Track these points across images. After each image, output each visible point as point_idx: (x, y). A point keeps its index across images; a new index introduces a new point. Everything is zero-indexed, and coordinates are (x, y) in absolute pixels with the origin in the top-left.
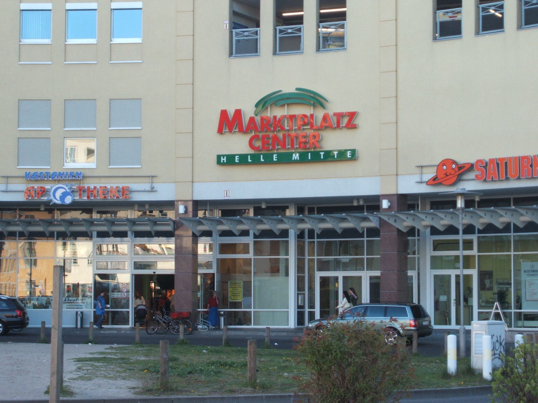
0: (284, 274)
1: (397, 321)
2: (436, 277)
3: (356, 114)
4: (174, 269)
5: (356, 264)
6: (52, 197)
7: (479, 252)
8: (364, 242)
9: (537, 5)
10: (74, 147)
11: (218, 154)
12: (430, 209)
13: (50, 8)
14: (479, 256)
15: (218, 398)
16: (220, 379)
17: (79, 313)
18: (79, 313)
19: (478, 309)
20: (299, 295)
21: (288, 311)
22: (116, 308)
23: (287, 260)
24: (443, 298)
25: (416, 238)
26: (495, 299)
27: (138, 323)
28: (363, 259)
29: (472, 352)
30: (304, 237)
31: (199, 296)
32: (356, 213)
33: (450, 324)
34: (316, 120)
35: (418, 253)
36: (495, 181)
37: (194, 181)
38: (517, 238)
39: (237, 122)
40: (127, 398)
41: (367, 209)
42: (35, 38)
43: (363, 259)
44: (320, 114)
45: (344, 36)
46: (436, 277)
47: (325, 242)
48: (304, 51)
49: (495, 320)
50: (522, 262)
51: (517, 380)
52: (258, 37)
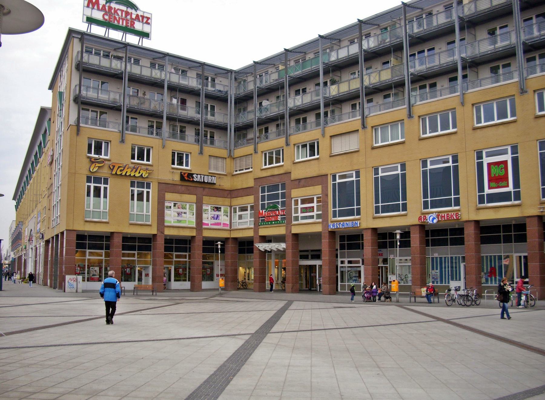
0: (531, 21)
1: (119, 293)
2: (104, 187)
3: (37, 276)
4: (138, 38)
5: (292, 352)
6: (428, 221)
7: (105, 257)
8: (454, 194)
9: (544, 204)
10: (363, 52)
11: (42, 106)
12: (106, 300)
13: (354, 148)
14: (137, 260)
15: (153, 269)
16: (37, 170)
17: (489, 283)
18: (489, 283)
19: (511, 155)
20: (131, 98)
21: (138, 238)
22: (110, 153)
23: (334, 206)
24: (133, 153)
25: (395, 249)
26: (437, 278)
27: (260, 230)
28: (381, 205)
29: (433, 88)
30: (399, 287)
31: (2, 263)
32: (516, 265)
33: (449, 129)
34: (517, 38)
35: (306, 208)
36: (244, 286)
37: (231, 231)
38: (504, 184)
39: (164, 56)
40: (384, 249)
41: (178, 121)
42: (493, 257)
43: (501, 235)
44: (134, 14)
45: (460, 33)
46: (104, 187)
47: (277, 156)
48: (362, 206)
49: (360, 97)
50: (285, 259)
51: (103, 203)
52: (501, 225)
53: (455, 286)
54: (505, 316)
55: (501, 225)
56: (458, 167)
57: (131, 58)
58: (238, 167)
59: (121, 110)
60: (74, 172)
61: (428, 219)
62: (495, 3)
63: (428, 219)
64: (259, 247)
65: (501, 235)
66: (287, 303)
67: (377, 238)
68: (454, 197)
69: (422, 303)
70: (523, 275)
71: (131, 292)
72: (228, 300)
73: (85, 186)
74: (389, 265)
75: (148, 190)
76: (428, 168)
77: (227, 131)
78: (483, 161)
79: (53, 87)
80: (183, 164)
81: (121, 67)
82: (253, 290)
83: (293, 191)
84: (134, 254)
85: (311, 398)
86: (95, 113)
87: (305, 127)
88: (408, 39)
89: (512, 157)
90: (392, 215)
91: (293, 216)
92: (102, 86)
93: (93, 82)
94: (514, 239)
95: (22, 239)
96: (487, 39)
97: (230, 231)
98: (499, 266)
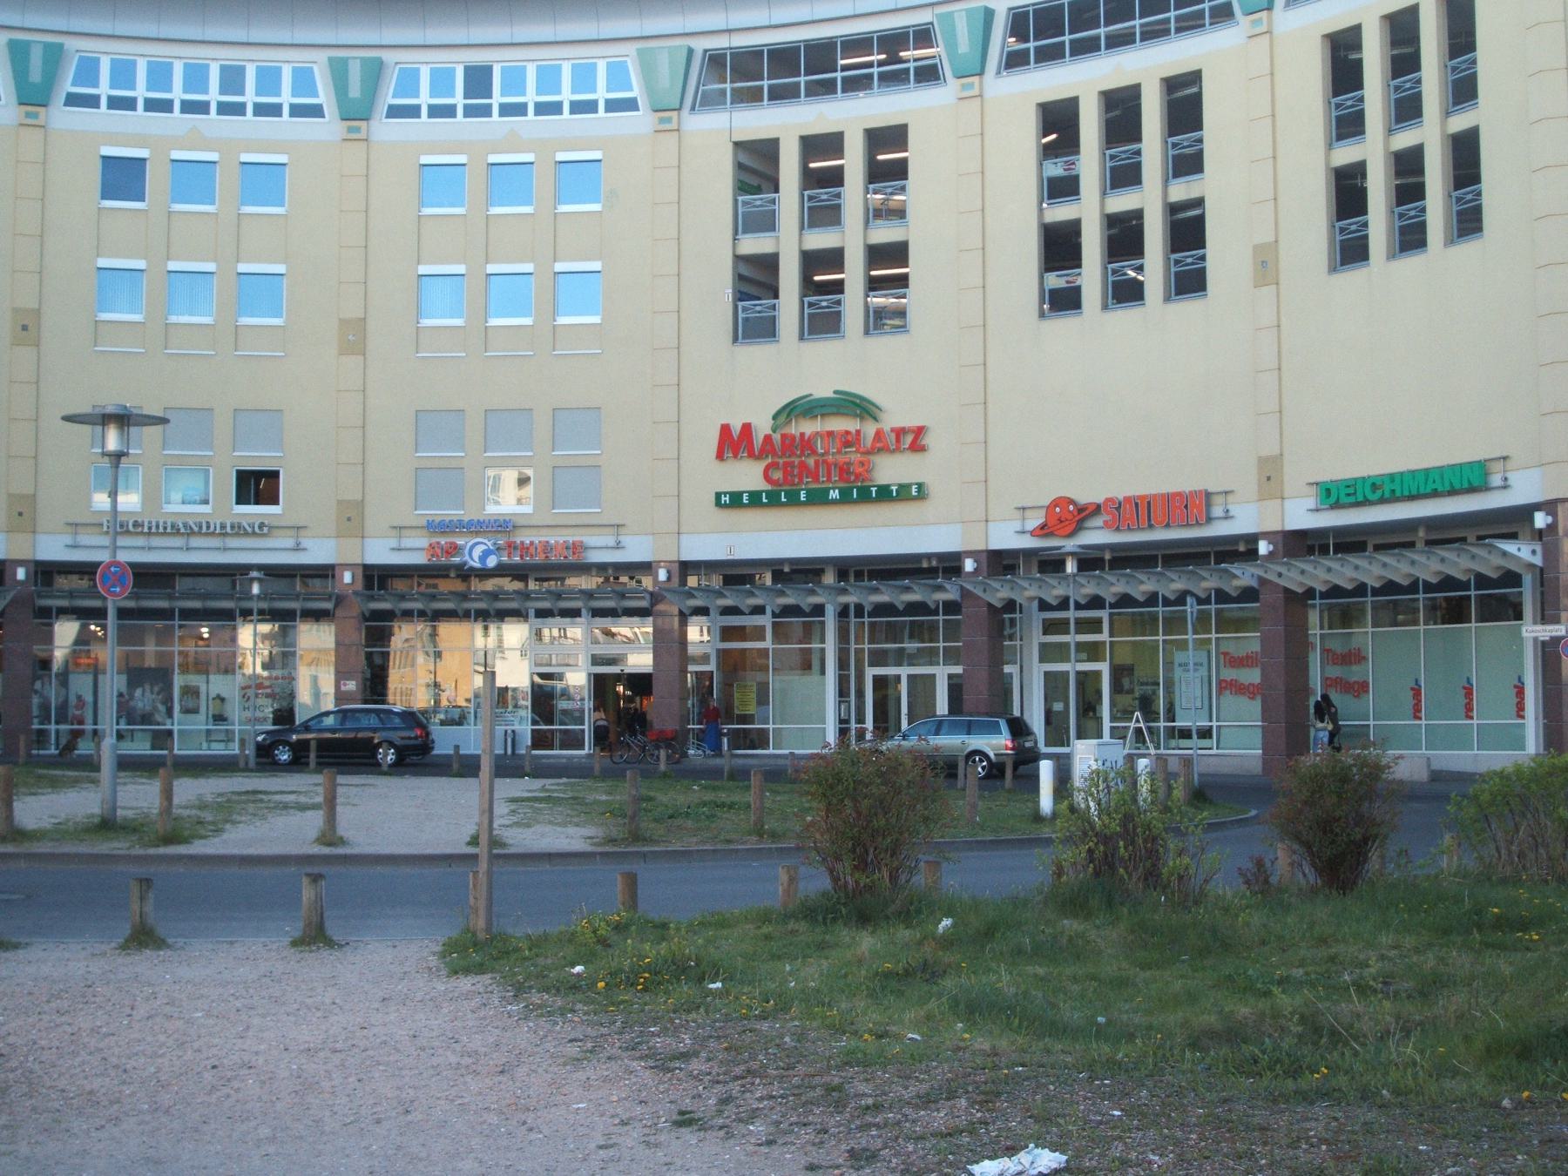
2: (1047, 674)
13: (283, 272)
18: (509, 732)
32: (1536, 699)
35: (818, 82)
39: (745, 443)
44: (870, 429)
46: (1047, 674)
52: (777, 313)
53: (1036, 314)
54: (36, 58)
55: (777, 313)
56: (1205, 272)
57: (257, 764)
58: (36, 721)
59: (214, 716)
60: (1286, 495)
61: (469, 560)
62: (1565, 556)
63: (469, 560)
64: (566, 557)
65: (1469, 597)
66: (731, 435)
67: (78, 820)
68: (1166, 15)
69: (242, 549)
70: (369, 754)
71: (565, 712)
72: (241, 546)
73: (181, 118)
74: (112, 726)
75: (460, 111)
76: (771, 647)
77: (746, 649)
78: (841, 168)
79: (1228, 548)
80: (1188, 646)
81: (641, 701)
82: (1201, 88)
83: (31, 80)
84: (1099, 621)
85: (987, 521)
86: (1223, 731)
87: (864, 409)
88: (1108, 165)
89: (824, 616)
90: (992, 37)
91: (1108, 662)
92: (1221, 697)
93: (818, 655)
94: (1505, 588)
95: (702, 864)
96: (68, 533)
97: (366, 540)
98: (848, 695)
